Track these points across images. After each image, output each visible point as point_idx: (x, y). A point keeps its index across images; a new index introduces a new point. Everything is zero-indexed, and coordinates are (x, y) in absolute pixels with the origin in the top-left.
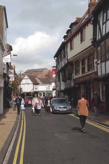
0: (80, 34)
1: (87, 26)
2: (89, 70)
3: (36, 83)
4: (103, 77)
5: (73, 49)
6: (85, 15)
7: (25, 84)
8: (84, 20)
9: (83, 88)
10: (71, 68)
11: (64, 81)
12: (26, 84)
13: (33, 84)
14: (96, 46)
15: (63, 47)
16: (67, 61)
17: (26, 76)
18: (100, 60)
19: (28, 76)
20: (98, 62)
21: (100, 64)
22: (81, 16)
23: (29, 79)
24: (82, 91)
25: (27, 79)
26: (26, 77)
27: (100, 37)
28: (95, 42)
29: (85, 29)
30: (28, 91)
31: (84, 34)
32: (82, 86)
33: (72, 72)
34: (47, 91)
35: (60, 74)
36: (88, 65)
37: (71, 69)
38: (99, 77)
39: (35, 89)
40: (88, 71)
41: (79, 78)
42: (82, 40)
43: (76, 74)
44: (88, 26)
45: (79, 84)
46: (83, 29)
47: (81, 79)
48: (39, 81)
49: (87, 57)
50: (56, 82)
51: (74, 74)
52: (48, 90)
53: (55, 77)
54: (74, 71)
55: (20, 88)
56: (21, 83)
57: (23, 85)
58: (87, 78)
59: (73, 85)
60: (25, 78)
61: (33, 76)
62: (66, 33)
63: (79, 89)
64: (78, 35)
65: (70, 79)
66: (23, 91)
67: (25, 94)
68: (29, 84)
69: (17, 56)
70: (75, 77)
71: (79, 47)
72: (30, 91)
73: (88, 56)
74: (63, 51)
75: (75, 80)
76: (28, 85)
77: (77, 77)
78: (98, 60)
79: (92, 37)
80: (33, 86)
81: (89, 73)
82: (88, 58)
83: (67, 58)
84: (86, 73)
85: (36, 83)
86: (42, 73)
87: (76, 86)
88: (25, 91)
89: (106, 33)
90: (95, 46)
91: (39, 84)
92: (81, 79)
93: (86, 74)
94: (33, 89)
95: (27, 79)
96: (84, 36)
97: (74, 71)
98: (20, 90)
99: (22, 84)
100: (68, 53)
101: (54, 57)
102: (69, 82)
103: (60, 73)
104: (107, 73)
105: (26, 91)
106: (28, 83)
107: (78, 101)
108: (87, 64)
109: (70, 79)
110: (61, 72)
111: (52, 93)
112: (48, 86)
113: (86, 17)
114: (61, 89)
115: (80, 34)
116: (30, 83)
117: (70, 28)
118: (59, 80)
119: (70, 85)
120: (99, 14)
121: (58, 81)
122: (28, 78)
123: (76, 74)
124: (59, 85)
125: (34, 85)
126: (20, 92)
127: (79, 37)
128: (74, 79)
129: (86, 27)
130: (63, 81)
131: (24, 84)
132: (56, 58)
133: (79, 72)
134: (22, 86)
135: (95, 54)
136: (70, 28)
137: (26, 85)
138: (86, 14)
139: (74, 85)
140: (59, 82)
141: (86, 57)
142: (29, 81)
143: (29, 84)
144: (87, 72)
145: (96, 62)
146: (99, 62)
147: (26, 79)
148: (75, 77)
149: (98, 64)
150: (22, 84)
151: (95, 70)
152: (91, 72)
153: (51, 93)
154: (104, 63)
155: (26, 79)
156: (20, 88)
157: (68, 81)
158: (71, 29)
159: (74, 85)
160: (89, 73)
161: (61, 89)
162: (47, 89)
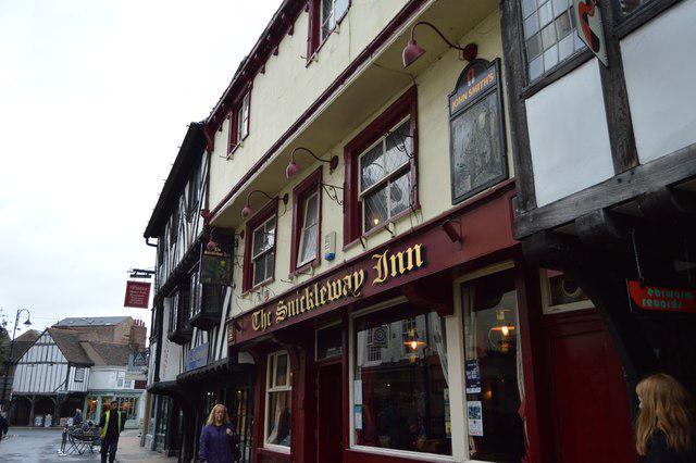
2: (353, 232)
10: (223, 258)
13: (70, 365)
16: (202, 219)
23: (56, 347)
24: (275, 389)
25: (50, 344)
33: (229, 281)
37: (223, 263)
40: (346, 243)
41: (269, 305)
43: (248, 287)
45: (261, 348)
47: (281, 311)
48: (92, 355)
51: (239, 290)
57: (30, 368)
59: (225, 354)
60: (43, 342)
61: (76, 341)
63: (255, 375)
65: (209, 322)
68: (52, 363)
70: (240, 303)
76: (50, 368)
83: (203, 207)
87: (243, 359)
91: (93, 365)
92: (281, 311)
97: (239, 276)
99: (27, 363)
100: (211, 182)
101: (147, 235)
102: (205, 340)
103: (165, 304)
104: (650, 147)
106: (49, 360)
107: (636, 450)
111: (137, 399)
114: (162, 379)
122: (52, 341)
123: (248, 287)
125: (73, 369)
130: (173, 339)
131: (33, 364)
132: (153, 241)
140: (155, 345)
142: (57, 354)
143: (52, 363)
147: (45, 344)
148: (240, 303)
155: (45, 344)
157: (200, 338)
159: (233, 351)
161: (162, 379)
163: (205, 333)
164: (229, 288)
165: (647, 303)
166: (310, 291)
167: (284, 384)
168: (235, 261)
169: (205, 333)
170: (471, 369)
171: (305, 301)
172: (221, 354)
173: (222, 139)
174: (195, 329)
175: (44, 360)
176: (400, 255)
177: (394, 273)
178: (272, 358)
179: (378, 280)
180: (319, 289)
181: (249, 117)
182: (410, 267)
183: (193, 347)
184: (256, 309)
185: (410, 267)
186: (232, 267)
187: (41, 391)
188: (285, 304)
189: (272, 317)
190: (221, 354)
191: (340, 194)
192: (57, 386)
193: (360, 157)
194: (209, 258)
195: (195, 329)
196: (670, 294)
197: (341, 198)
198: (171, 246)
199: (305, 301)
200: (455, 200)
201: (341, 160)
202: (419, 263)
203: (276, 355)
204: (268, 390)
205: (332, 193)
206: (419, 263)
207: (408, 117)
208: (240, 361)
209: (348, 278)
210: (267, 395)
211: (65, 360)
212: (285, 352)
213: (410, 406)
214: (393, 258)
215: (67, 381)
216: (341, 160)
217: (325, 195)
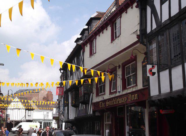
0: (109, 28)
1: (130, 8)
2: (124, 88)
3: (29, 109)
4: (163, 98)
5: (96, 53)
6: (112, 7)
7: (14, 109)
8: (110, 14)
9: (108, 117)
11: (75, 106)
12: (15, 109)
13: (26, 110)
14: (145, 43)
15: (76, 56)
17: (16, 97)
18: (156, 66)
19: (19, 98)
20: (153, 71)
21: (156, 75)
22: (104, 10)
24: (107, 123)
25: (17, 102)
26: (16, 99)
27: (154, 26)
28: (144, 37)
29: (121, 17)
30: (18, 119)
31: (94, 45)
32: (106, 114)
34: (45, 120)
35: (68, 95)
36: (123, 80)
37: (90, 86)
38: (153, 99)
39: (28, 116)
41: (104, 101)
42: (91, 54)
43: (97, 95)
44: (103, 33)
45: (102, 111)
46: (93, 41)
47: (108, 103)
48: (34, 106)
49: (124, 66)
50: (59, 108)
51: (95, 95)
52: (45, 118)
53: (58, 100)
54: (94, 90)
55: (7, 115)
56: (9, 108)
57: (11, 111)
58: (120, 101)
59: (91, 113)
61: (27, 97)
62: (86, 25)
63: (100, 119)
64: (87, 46)
66: (11, 119)
67: (14, 123)
68: (19, 109)
69: (3, 65)
71: (105, 47)
72: (20, 119)
73: (122, 64)
74: (76, 59)
75: (96, 105)
76: (19, 111)
77: (100, 99)
78: (153, 67)
79: (138, 28)
80: (26, 113)
81: (124, 93)
82: (124, 65)
84: (119, 92)
85: (29, 109)
86: (38, 95)
87: (97, 114)
88: (13, 119)
89: (172, 15)
90: (144, 42)
91: (34, 109)
93: (118, 94)
94: (25, 116)
95: (17, 102)
96: (94, 48)
97: (94, 90)
98: (7, 117)
99: (10, 109)
102: (84, 108)
105: (14, 119)
106: (18, 108)
108: (95, 87)
109: (86, 102)
110: (70, 91)
111: (51, 123)
112: (45, 113)
113: (113, 10)
114: (70, 119)
115: (109, 28)
116: (22, 108)
117: (86, 27)
118: (66, 105)
119: (86, 112)
120: (95, 40)
121: (64, 107)
123: (97, 95)
124: (66, 111)
125: (27, 111)
126: (6, 121)
127: (108, 33)
128: (94, 103)
129: (98, 37)
130: (73, 106)
131: (12, 109)
132: (62, 71)
133: (104, 91)
134: (9, 112)
135: (138, 59)
136: (86, 27)
137: (15, 110)
138: (113, 6)
139: (93, 111)
140: (66, 108)
141: (119, 67)
142: (20, 105)
143: (19, 109)
144: (120, 90)
145: (150, 70)
146: (155, 70)
149: (154, 74)
150: (10, 109)
151: (140, 86)
152: (129, 91)
153: (49, 123)
154: (167, 71)
156: (7, 115)
157: (82, 107)
158: (88, 27)
160: (125, 93)
161: (70, 119)
162: (45, 117)
163: (84, 105)
164: (91, 94)
165: (163, 113)
166: (115, 99)
167: (109, 122)
168: (93, 86)
169: (84, 105)
170: (48, 109)
171: (113, 102)
172: (90, 112)
173: (87, 49)
174: (80, 104)
175: (16, 108)
176: (134, 96)
177: (132, 99)
178: (105, 114)
179: (129, 100)
180: (117, 100)
181: (96, 46)
182: (135, 99)
183: (80, 109)
184: (101, 101)
185: (135, 99)
186: (92, 88)
187: (16, 120)
188: (108, 102)
189: (105, 105)
190: (90, 112)
191: (121, 76)
192: (22, 118)
193: (125, 67)
194: (86, 85)
195: (80, 104)
196: (165, 111)
197: (121, 78)
198: (71, 76)
199: (113, 102)
200: (143, 86)
201: (121, 67)
202: (137, 98)
203: (107, 113)
204: (105, 123)
205: (119, 77)
206: (137, 98)
207: (135, 62)
208: (96, 115)
209: (123, 98)
210: (104, 124)
211: (24, 108)
212: (109, 113)
213: (137, 122)
214: (132, 96)
215: (25, 116)
216: (121, 67)
217: (117, 78)
